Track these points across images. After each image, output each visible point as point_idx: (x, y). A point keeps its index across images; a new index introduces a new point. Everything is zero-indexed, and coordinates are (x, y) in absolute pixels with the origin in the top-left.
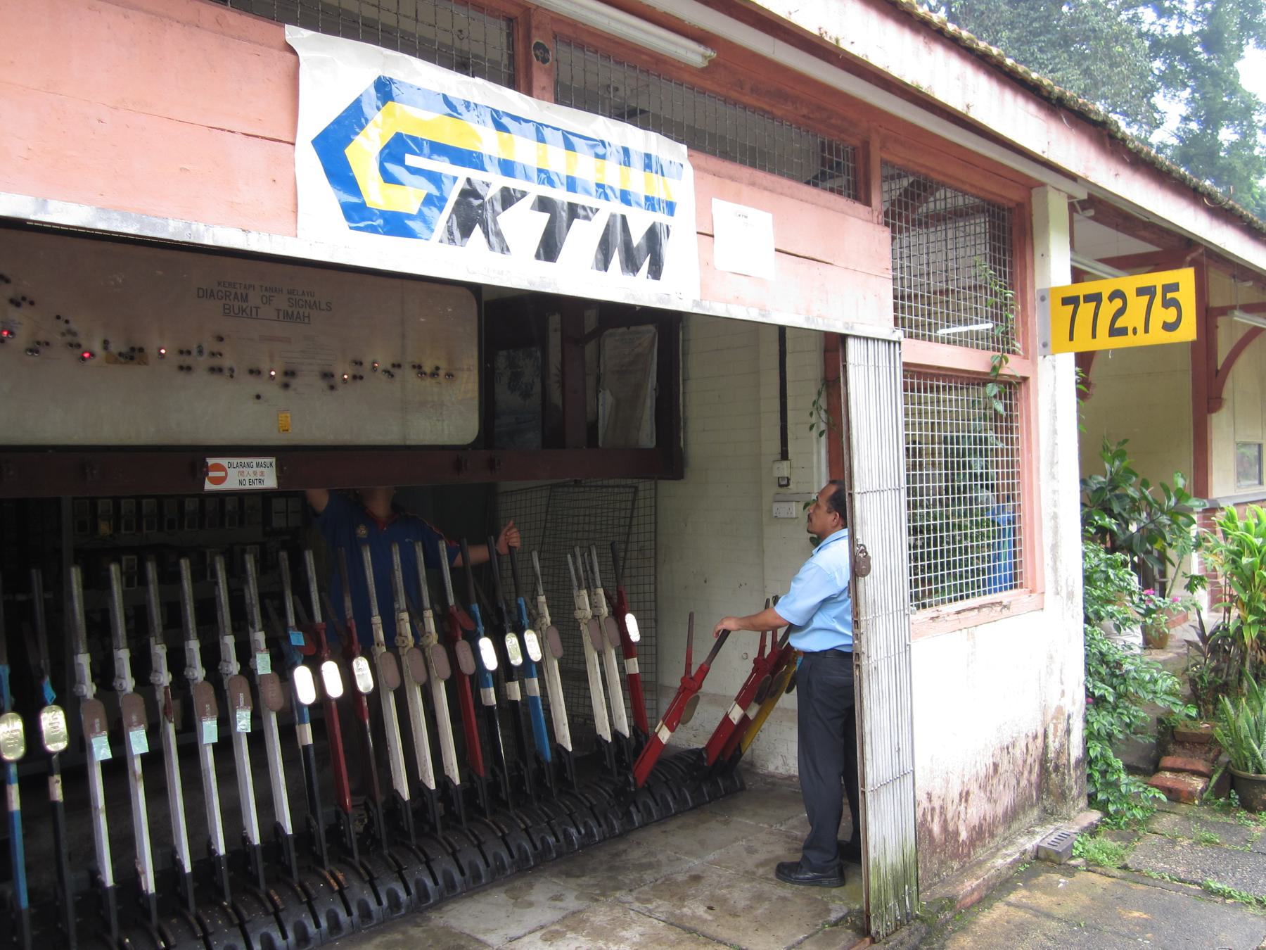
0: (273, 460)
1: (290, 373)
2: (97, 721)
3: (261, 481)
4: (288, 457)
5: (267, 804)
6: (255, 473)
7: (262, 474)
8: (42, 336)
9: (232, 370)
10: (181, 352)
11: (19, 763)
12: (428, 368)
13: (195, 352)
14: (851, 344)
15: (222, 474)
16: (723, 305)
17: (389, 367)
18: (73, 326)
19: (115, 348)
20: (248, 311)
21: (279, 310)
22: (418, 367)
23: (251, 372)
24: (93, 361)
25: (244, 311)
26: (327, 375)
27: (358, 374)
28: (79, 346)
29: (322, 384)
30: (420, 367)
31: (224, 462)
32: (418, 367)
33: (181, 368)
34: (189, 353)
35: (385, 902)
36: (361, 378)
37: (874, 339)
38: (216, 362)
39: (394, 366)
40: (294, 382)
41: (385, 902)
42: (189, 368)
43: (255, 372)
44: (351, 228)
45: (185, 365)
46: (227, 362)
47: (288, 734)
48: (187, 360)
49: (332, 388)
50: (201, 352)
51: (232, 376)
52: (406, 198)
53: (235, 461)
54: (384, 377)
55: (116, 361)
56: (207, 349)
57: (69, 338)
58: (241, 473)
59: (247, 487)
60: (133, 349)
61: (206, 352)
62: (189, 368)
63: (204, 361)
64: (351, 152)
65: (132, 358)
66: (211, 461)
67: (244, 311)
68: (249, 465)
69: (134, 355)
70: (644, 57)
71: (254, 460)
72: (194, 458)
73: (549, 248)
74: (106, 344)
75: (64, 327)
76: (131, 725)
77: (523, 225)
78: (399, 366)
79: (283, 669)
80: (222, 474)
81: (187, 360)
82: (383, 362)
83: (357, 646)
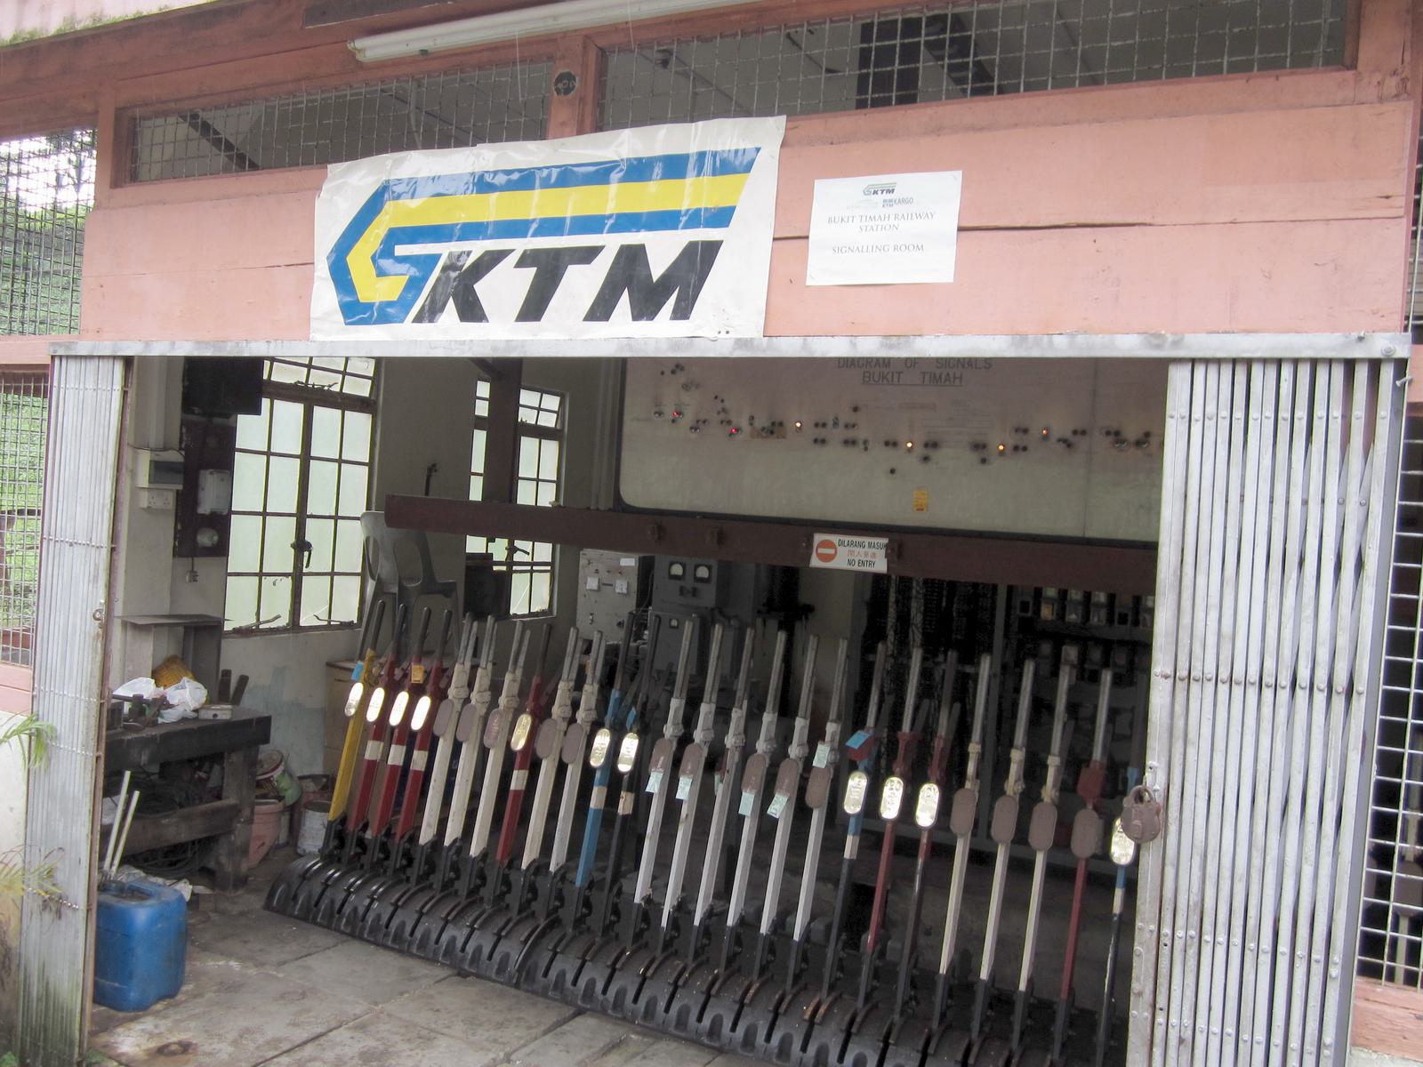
0: (885, 541)
1: (933, 445)
2: (662, 758)
3: (871, 563)
4: (899, 538)
5: (792, 899)
6: (866, 555)
7: (874, 555)
8: (702, 417)
9: (865, 442)
10: (816, 425)
11: (858, 815)
12: (1131, 433)
13: (830, 424)
14: (1178, 378)
15: (831, 551)
16: (798, 341)
17: (1068, 434)
18: (727, 404)
19: (758, 424)
20: (889, 377)
21: (924, 373)
22: (1116, 436)
23: (887, 444)
24: (740, 437)
25: (884, 377)
26: (979, 447)
27: (1021, 444)
28: (729, 422)
29: (974, 457)
30: (1117, 433)
31: (835, 538)
32: (1116, 436)
33: (846, 442)
34: (824, 425)
35: (707, 1022)
36: (1025, 449)
37: (1207, 361)
38: (850, 434)
39: (1075, 432)
40: (936, 455)
41: (707, 1022)
42: (823, 441)
43: (892, 444)
44: (346, 324)
45: (820, 438)
46: (861, 434)
47: (832, 844)
48: (821, 433)
49: (984, 461)
50: (836, 424)
51: (866, 449)
52: (386, 289)
53: (847, 538)
54: (1061, 447)
55: (759, 435)
56: (843, 419)
57: (722, 416)
58: (851, 553)
59: (856, 568)
60: (773, 424)
61: (841, 424)
62: (823, 441)
63: (841, 433)
64: (351, 259)
65: (772, 432)
66: (819, 538)
67: (884, 377)
68: (861, 545)
69: (775, 429)
70: (734, 17)
71: (866, 540)
72: (803, 529)
73: (534, 308)
74: (752, 418)
75: (720, 406)
76: (684, 773)
77: (505, 288)
78: (1084, 433)
79: (843, 767)
80: (831, 551)
81: (821, 433)
82: (1061, 428)
83: (935, 769)
